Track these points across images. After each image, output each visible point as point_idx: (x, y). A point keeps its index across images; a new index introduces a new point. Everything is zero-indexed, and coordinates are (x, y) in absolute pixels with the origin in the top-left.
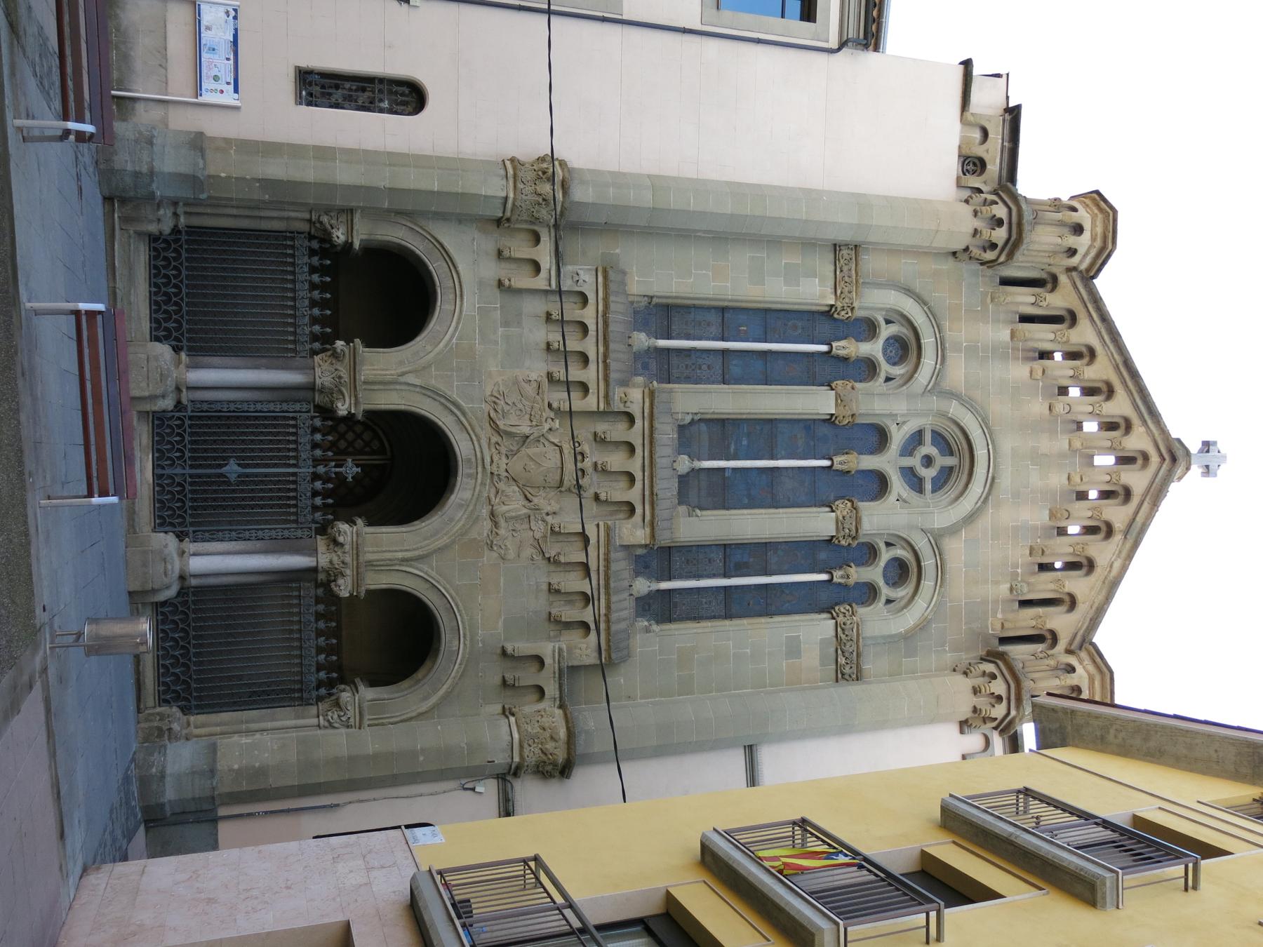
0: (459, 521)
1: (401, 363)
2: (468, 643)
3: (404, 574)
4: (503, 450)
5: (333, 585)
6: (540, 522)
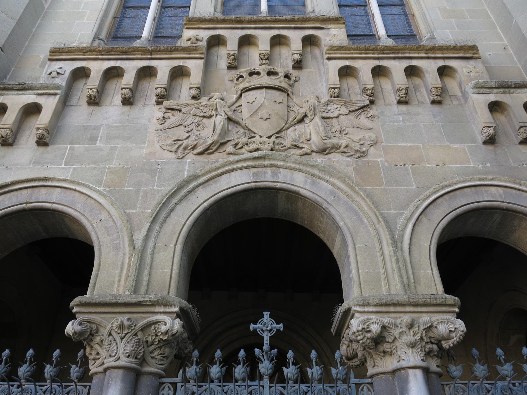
0: (333, 185)
1: (117, 248)
2: (490, 177)
3: (414, 248)
4: (243, 140)
5: (445, 345)
6: (329, 108)
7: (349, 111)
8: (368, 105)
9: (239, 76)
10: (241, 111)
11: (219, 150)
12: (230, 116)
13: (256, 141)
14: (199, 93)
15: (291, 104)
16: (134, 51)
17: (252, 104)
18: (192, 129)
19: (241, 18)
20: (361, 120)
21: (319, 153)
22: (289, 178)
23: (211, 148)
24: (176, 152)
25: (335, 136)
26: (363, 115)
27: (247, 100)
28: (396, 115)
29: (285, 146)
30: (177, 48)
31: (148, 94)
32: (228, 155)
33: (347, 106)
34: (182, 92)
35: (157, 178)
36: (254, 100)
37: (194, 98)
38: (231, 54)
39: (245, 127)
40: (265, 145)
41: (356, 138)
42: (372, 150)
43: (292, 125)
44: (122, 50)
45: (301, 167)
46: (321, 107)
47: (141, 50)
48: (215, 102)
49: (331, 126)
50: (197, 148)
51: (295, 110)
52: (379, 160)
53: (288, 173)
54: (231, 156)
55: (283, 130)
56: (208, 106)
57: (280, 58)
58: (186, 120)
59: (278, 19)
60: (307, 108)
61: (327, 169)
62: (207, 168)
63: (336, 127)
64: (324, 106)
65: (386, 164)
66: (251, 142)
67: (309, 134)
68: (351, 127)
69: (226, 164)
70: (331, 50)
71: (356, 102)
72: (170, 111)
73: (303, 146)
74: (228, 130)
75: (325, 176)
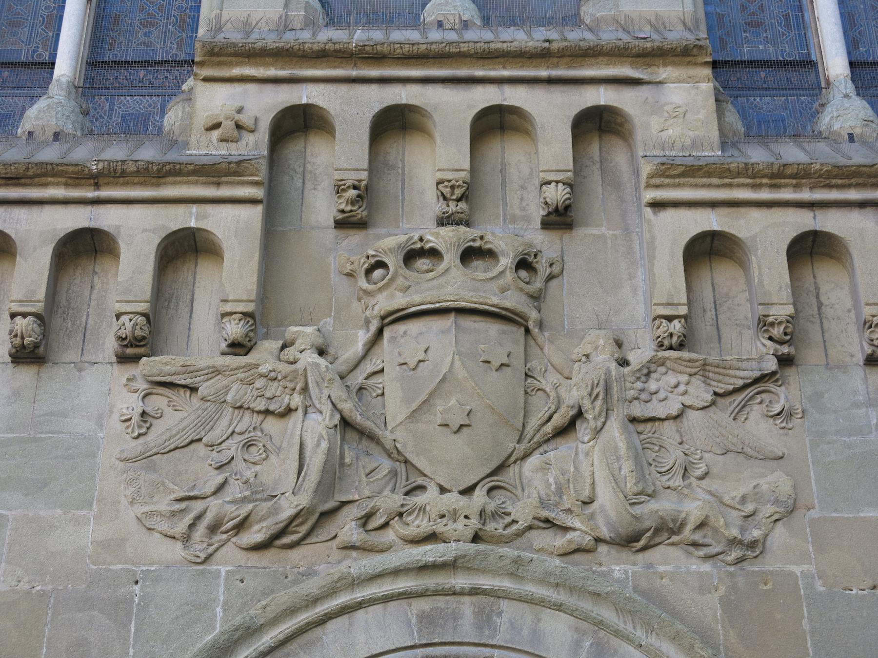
4: (390, 501)
6: (653, 386)
7: (715, 394)
8: (774, 373)
9: (372, 261)
10: (380, 392)
11: (315, 533)
12: (347, 414)
13: (428, 508)
14: (252, 330)
15: (534, 363)
16: (45, 175)
17: (414, 369)
18: (233, 458)
19: (379, 47)
20: (751, 425)
21: (619, 544)
22: (525, 632)
23: (291, 529)
24: (186, 538)
25: (669, 488)
26: (756, 407)
27: (400, 354)
28: (857, 405)
29: (514, 522)
30: (178, 167)
31: (90, 322)
32: (344, 552)
33: (708, 378)
34: (194, 315)
35: (133, 630)
36: (421, 356)
37: (238, 347)
38: (349, 183)
39: (395, 451)
40: (455, 521)
41: (733, 491)
42: (780, 536)
43: (539, 445)
44: (6, 173)
45: (561, 597)
46: (628, 385)
47: (66, 173)
48: (300, 365)
49: (657, 448)
50: (251, 526)
51: (548, 390)
52: (797, 570)
53: (524, 614)
54: (354, 554)
55: (509, 463)
56: (279, 378)
57: (504, 184)
58: (209, 423)
59: (496, 50)
60: (585, 392)
61: (638, 608)
62: (283, 598)
63: (671, 450)
64: (638, 378)
65: (819, 586)
66: (413, 511)
67: (588, 481)
68: (719, 452)
69: (339, 585)
70: (663, 175)
71: (735, 364)
72: (161, 390)
73: (569, 524)
74: (342, 464)
75: (634, 628)
